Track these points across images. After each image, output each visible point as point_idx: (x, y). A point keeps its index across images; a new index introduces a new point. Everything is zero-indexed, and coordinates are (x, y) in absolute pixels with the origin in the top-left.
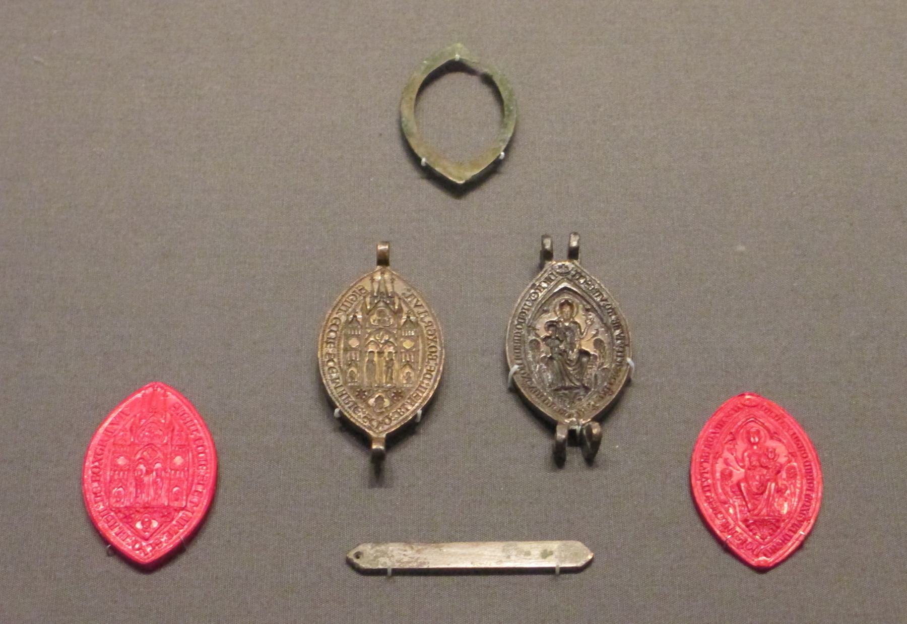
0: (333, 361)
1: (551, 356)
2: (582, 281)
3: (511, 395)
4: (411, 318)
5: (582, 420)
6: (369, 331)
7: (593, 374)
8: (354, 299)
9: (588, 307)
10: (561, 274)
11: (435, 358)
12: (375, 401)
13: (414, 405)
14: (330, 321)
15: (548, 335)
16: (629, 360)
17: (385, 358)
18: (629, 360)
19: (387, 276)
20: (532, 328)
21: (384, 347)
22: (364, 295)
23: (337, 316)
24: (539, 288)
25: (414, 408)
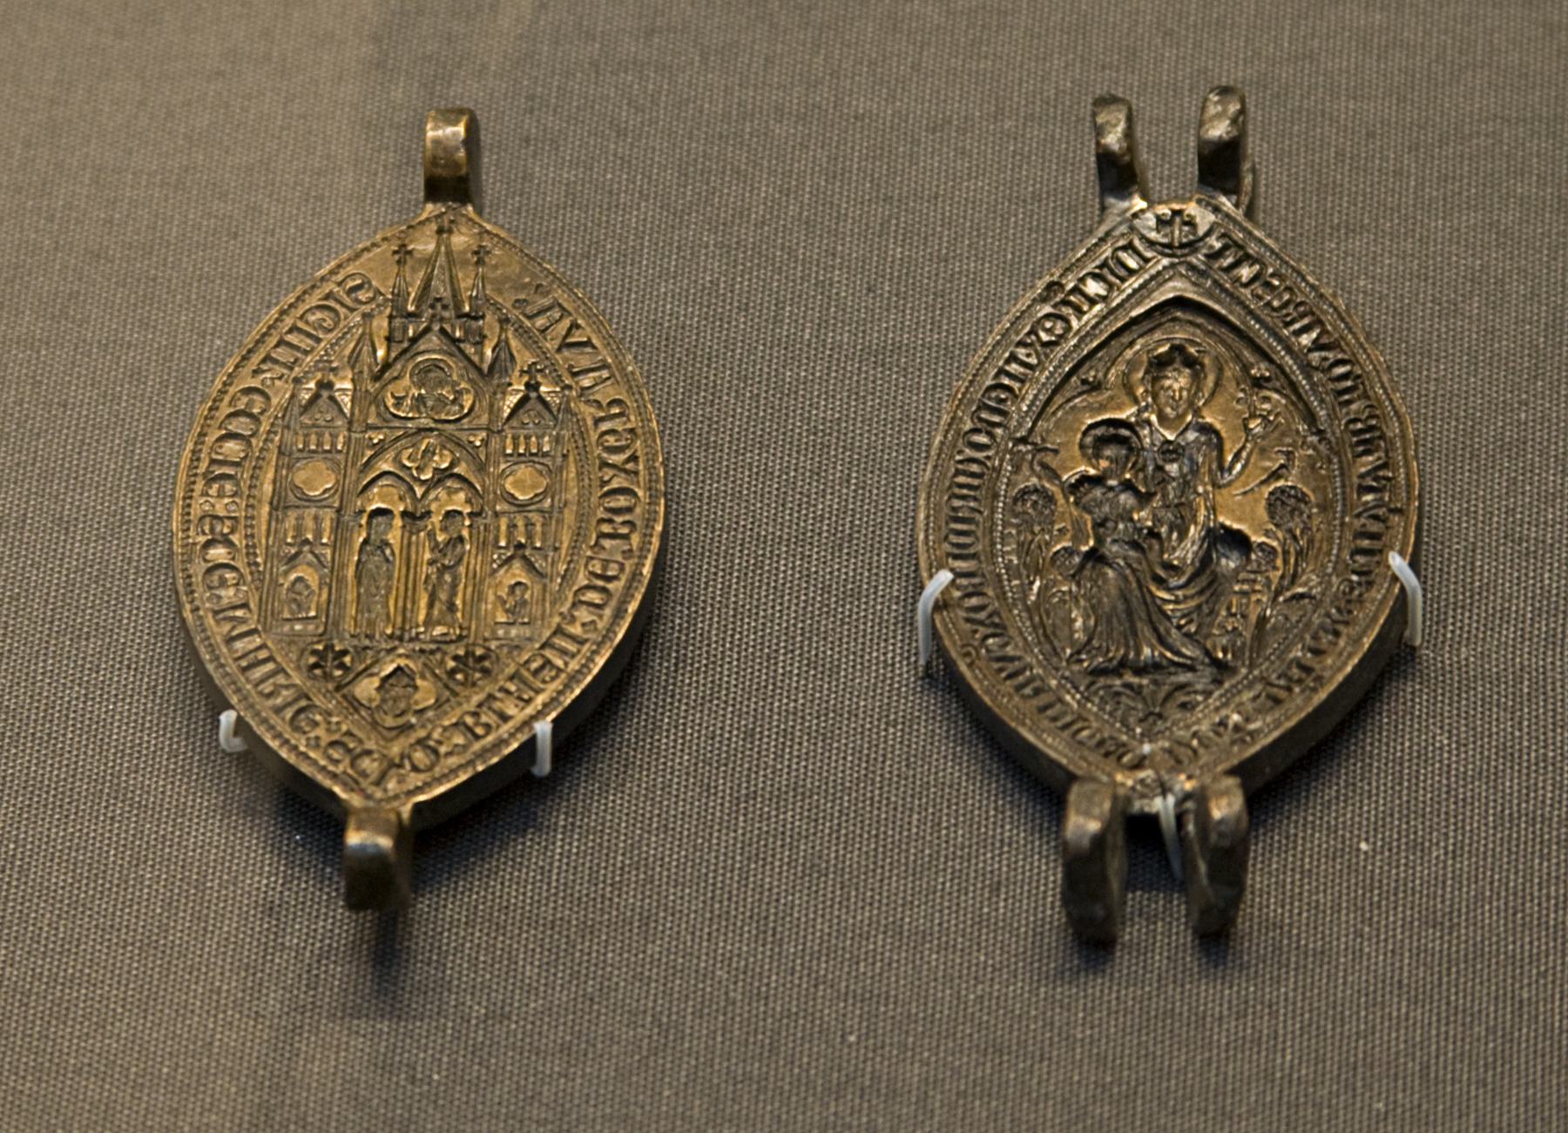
0: (228, 543)
1: (1093, 551)
2: (1245, 272)
3: (932, 701)
4: (543, 389)
5: (1183, 777)
6: (377, 437)
7: (1253, 618)
8: (329, 323)
9: (1260, 369)
10: (1167, 249)
11: (624, 530)
12: (379, 689)
13: (529, 701)
14: (227, 399)
15: (1092, 472)
16: (1397, 562)
17: (431, 535)
18: (1397, 562)
19: (460, 240)
20: (1035, 448)
21: (432, 496)
22: (366, 309)
23: (255, 383)
24: (1076, 300)
25: (530, 710)
